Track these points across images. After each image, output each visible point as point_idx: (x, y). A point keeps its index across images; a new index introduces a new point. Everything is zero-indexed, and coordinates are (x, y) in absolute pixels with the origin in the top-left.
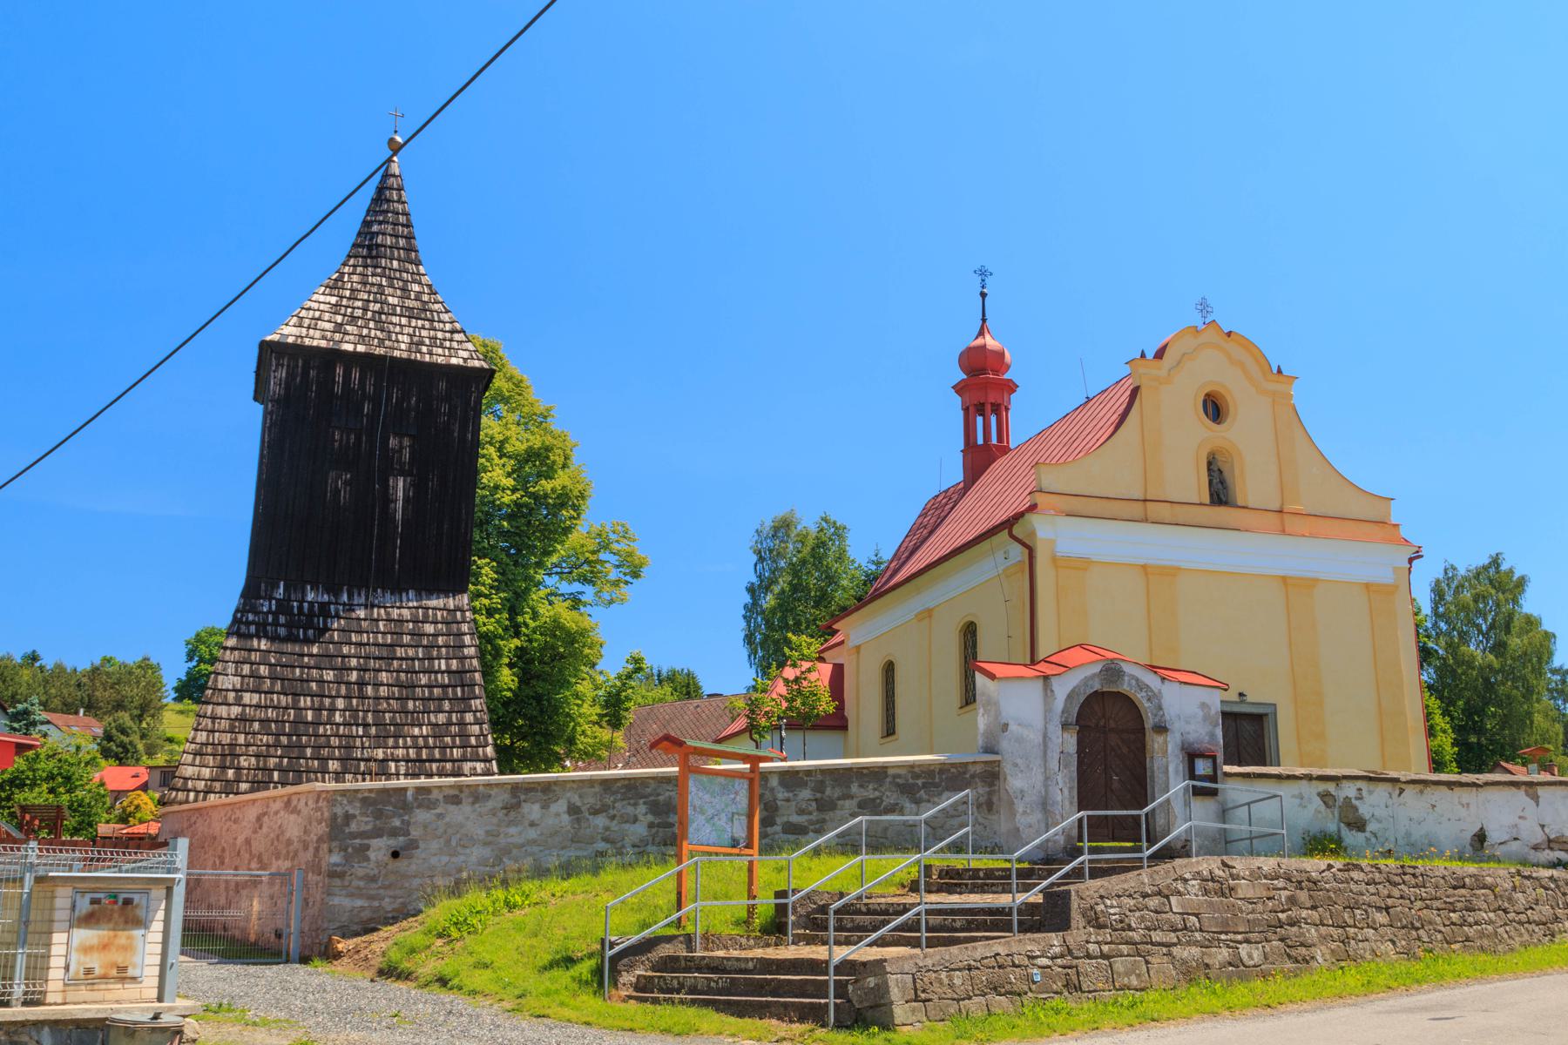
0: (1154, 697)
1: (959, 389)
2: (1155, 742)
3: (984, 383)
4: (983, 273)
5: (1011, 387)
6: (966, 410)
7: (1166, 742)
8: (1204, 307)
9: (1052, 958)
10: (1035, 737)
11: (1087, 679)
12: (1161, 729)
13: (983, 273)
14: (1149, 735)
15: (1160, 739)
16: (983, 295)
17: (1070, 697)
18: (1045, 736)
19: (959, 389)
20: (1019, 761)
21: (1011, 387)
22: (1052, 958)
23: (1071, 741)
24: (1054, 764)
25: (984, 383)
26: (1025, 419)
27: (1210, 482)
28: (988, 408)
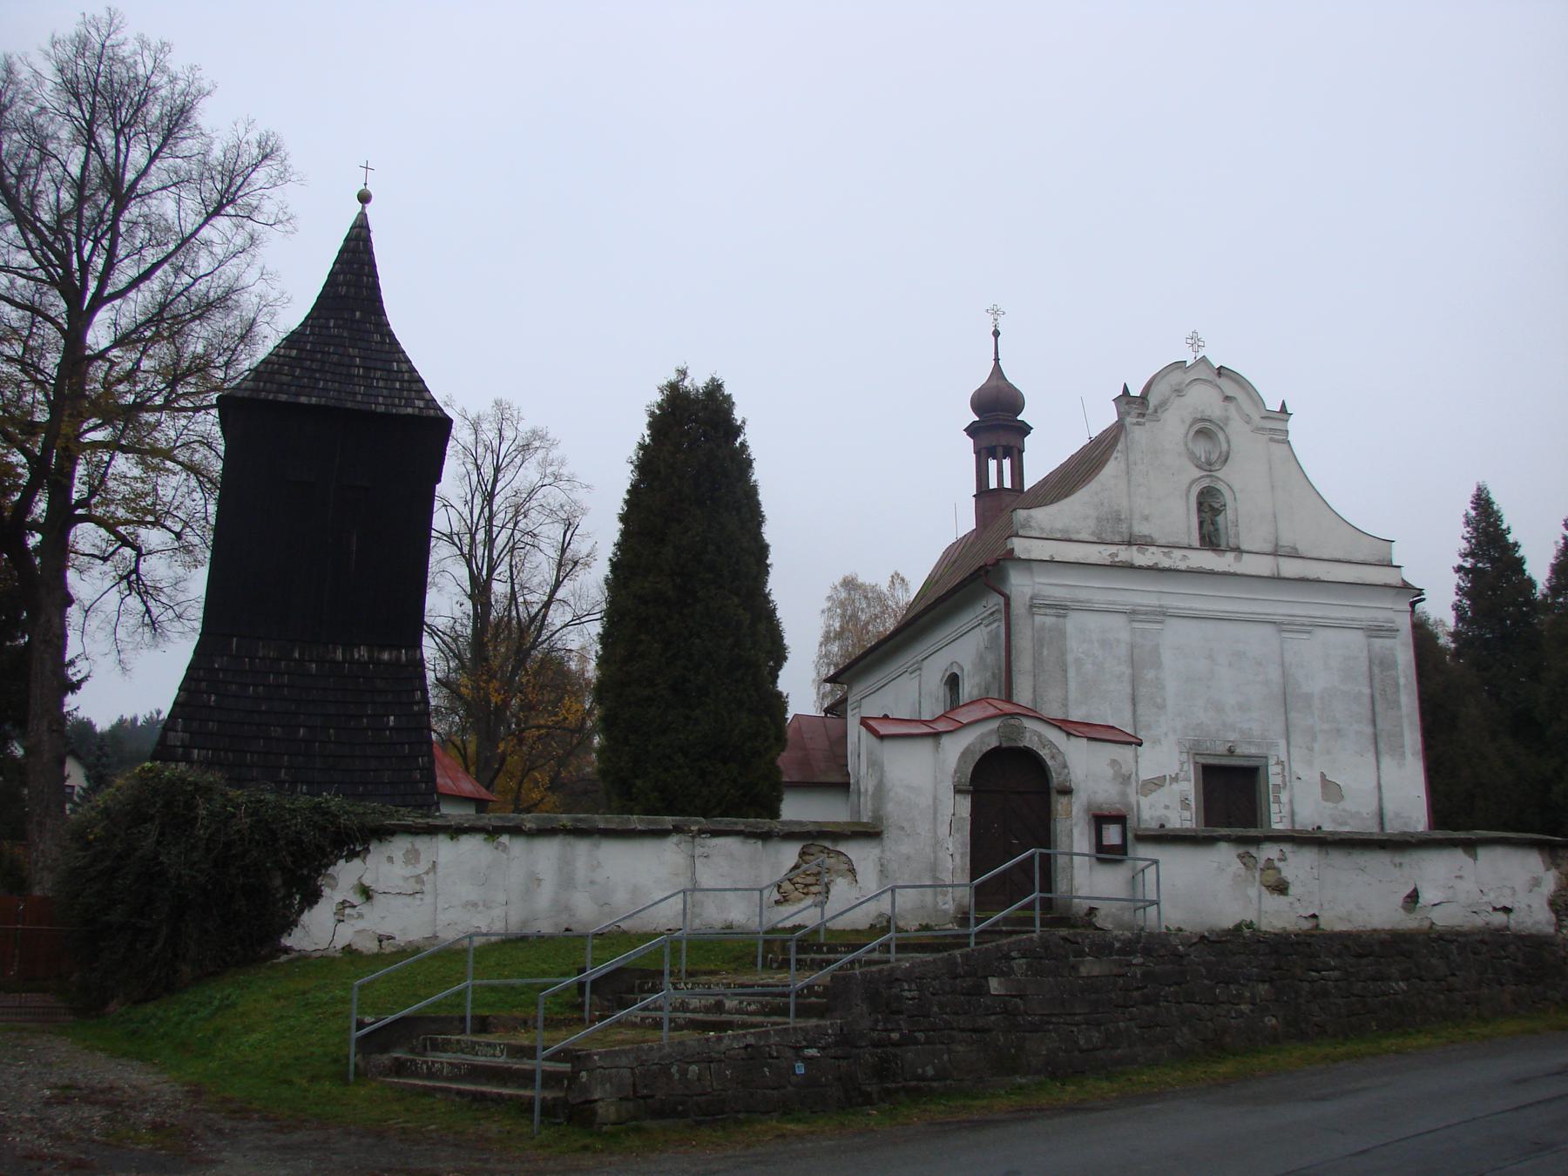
0: (1057, 753)
1: (972, 431)
2: (1060, 804)
3: (998, 420)
4: (996, 312)
5: (1025, 430)
6: (977, 452)
7: (1070, 804)
8: (1195, 341)
9: (823, 1049)
10: (925, 801)
11: (983, 736)
12: (1067, 791)
13: (996, 312)
14: (1054, 796)
15: (1063, 800)
16: (996, 334)
17: (964, 754)
18: (935, 798)
19: (972, 431)
20: (905, 825)
21: (1025, 430)
22: (823, 1049)
23: (965, 805)
24: (944, 829)
25: (998, 420)
26: (1041, 458)
27: (1201, 524)
28: (1000, 451)
